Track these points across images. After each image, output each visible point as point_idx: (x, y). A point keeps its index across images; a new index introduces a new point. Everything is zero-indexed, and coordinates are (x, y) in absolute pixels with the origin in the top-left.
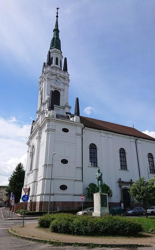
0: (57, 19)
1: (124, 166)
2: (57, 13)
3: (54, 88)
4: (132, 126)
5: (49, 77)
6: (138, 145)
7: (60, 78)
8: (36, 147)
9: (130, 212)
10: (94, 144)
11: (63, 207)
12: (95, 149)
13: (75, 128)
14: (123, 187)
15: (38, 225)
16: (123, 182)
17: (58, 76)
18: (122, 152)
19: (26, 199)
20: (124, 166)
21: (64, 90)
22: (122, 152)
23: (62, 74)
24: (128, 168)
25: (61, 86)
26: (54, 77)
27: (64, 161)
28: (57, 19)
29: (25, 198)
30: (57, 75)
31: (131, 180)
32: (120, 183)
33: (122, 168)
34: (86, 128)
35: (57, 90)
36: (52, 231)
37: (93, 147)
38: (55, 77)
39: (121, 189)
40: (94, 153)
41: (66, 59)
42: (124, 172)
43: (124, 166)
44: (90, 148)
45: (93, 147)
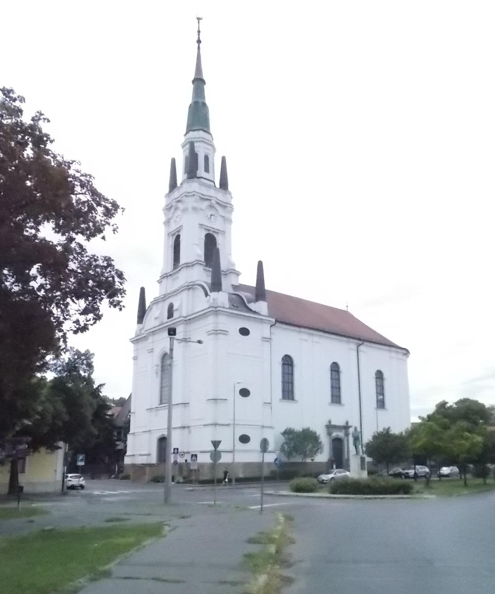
0: (199, 48)
1: (336, 398)
4: (343, 308)
5: (196, 205)
7: (217, 206)
9: (26, 296)
14: (334, 434)
18: (335, 369)
21: (224, 232)
22: (335, 369)
23: (220, 196)
24: (297, 395)
26: (206, 204)
27: (245, 393)
28: (199, 48)
30: (210, 200)
31: (347, 423)
32: (330, 427)
35: (211, 232)
37: (288, 362)
39: (330, 438)
42: (336, 408)
43: (336, 398)
45: (288, 362)
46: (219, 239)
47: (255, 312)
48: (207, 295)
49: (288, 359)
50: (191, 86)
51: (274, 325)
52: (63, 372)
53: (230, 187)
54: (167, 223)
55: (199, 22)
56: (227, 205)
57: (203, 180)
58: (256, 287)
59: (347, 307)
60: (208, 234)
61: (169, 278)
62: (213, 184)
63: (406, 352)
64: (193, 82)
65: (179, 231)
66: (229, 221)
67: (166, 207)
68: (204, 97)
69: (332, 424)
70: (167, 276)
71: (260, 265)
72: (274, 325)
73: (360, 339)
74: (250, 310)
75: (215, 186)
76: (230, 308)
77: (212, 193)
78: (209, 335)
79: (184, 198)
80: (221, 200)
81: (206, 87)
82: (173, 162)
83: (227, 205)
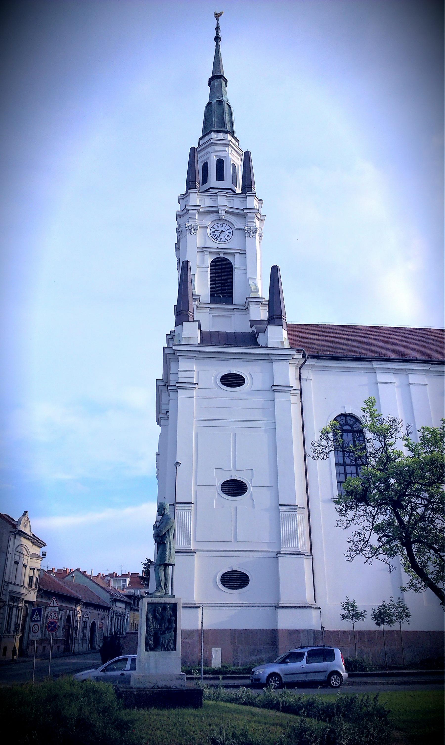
0: (217, 22)
2: (217, 29)
8: (139, 624)
11: (236, 651)
12: (357, 435)
13: (268, 365)
17: (220, 212)
34: (310, 362)
35: (222, 255)
38: (213, 217)
40: (340, 473)
46: (236, 263)
57: (211, 190)
60: (217, 258)
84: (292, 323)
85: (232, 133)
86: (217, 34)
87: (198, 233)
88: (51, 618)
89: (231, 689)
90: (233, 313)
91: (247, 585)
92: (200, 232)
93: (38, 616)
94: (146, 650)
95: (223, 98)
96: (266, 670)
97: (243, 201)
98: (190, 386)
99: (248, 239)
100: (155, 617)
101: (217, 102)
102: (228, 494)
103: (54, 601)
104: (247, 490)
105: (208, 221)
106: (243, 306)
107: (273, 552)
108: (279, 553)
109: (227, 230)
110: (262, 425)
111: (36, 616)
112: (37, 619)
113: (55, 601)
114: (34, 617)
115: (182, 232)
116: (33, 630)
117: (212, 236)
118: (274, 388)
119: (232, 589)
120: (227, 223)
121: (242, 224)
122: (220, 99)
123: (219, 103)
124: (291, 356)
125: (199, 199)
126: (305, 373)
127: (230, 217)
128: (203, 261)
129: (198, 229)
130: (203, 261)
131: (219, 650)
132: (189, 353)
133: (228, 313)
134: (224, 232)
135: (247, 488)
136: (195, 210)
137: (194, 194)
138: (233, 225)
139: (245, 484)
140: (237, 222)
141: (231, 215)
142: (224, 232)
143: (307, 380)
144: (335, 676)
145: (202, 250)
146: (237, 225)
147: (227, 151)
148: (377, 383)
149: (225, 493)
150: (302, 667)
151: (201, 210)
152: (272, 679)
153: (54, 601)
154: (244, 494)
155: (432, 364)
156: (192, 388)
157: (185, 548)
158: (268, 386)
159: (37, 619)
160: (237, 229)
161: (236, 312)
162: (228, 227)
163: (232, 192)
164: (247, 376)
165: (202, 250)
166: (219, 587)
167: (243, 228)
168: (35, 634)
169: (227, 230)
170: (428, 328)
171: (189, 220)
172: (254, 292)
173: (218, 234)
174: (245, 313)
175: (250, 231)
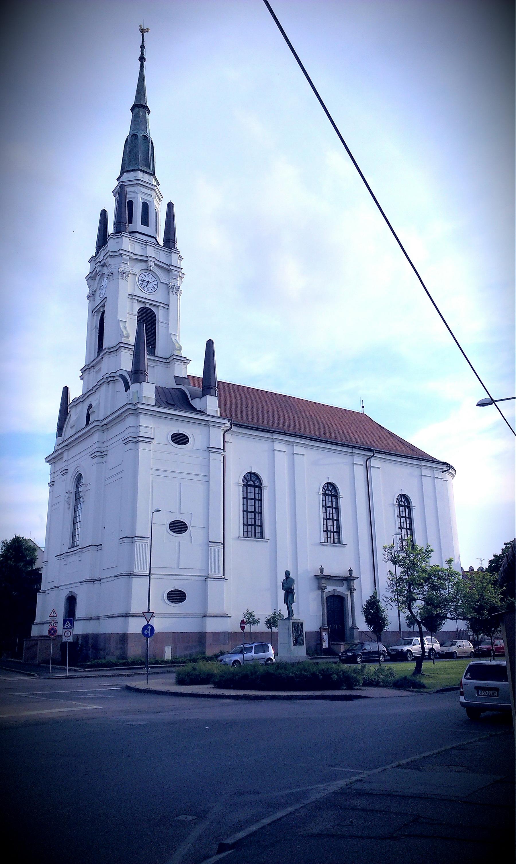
0: (142, 67)
2: (143, 47)
3: (138, 301)
4: (357, 409)
6: (374, 474)
7: (156, 269)
10: (255, 474)
12: (257, 489)
13: (205, 429)
14: (330, 589)
15: (174, 681)
16: (330, 579)
19: (149, 632)
20: (255, 499)
23: (162, 257)
25: (158, 296)
28: (142, 67)
29: (148, 631)
30: (146, 261)
31: (350, 571)
33: (247, 534)
34: (234, 429)
35: (148, 306)
36: (96, 647)
38: (142, 265)
41: (170, 206)
42: (332, 551)
44: (244, 485)
46: (160, 315)
47: (201, 412)
48: (127, 388)
49: (254, 478)
50: (130, 115)
51: (230, 429)
52: (415, 571)
53: (179, 245)
54: (91, 296)
55: (143, 35)
56: (171, 267)
57: (138, 236)
58: (203, 378)
59: (363, 407)
60: (143, 307)
61: (92, 370)
62: (153, 240)
63: (448, 467)
64: (132, 110)
65: (103, 306)
66: (177, 290)
67: (90, 275)
68: (146, 129)
69: (325, 573)
70: (89, 369)
71: (210, 345)
72: (230, 429)
73: (370, 450)
74: (193, 409)
75: (159, 244)
76: (156, 405)
77: (151, 251)
78: (125, 444)
79: (109, 259)
80: (166, 263)
81: (150, 118)
82: (104, 213)
83: (171, 267)
84: (193, 375)
85: (153, 174)
86: (142, 54)
87: (129, 279)
88: (52, 625)
89: (215, 672)
90: (156, 364)
91: (184, 600)
92: (130, 278)
93: (70, 625)
94: (293, 645)
95: (147, 133)
96: (232, 658)
97: (168, 256)
98: (149, 440)
99: (171, 295)
100: (295, 629)
101: (143, 136)
102: (174, 532)
103: (53, 612)
104: (187, 529)
105: (138, 268)
106: (166, 360)
107: (204, 576)
108: (207, 578)
109: (153, 281)
110: (200, 478)
111: (68, 624)
112: (68, 627)
113: (54, 612)
114: (66, 625)
115: (112, 274)
116: (66, 635)
117: (140, 284)
118: (210, 449)
119: (174, 603)
120: (150, 272)
121: (167, 279)
122: (145, 135)
123: (144, 138)
124: (224, 424)
125: (131, 244)
126: (228, 436)
127: (157, 269)
128: (132, 309)
129: (129, 276)
130: (132, 309)
131: (170, 647)
132: (146, 411)
133: (153, 364)
134: (151, 282)
135: (187, 528)
136: (128, 255)
137: (127, 238)
138: (159, 278)
139: (186, 524)
140: (163, 277)
141: (157, 267)
142: (151, 282)
143: (228, 442)
144: (269, 661)
145: (131, 297)
146: (163, 279)
147: (152, 196)
148: (274, 450)
149: (172, 531)
150: (252, 656)
151: (134, 257)
152: (235, 664)
153: (53, 612)
154: (185, 532)
155: (310, 440)
156: (150, 443)
157: (143, 572)
158: (205, 447)
159: (68, 627)
160: (162, 283)
161: (159, 364)
162: (154, 279)
163: (157, 244)
164: (191, 437)
165: (131, 297)
166: (166, 601)
167: (168, 283)
168: (68, 638)
169: (153, 281)
170: (290, 396)
171: (122, 265)
172: (178, 350)
173: (145, 284)
174: (166, 366)
175: (174, 288)
